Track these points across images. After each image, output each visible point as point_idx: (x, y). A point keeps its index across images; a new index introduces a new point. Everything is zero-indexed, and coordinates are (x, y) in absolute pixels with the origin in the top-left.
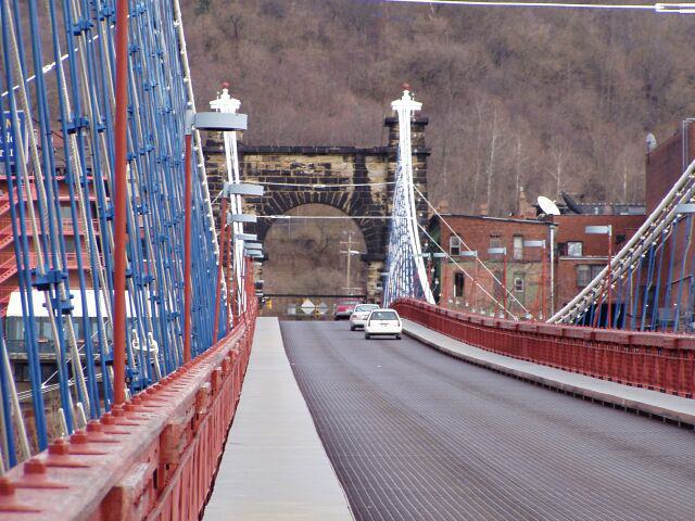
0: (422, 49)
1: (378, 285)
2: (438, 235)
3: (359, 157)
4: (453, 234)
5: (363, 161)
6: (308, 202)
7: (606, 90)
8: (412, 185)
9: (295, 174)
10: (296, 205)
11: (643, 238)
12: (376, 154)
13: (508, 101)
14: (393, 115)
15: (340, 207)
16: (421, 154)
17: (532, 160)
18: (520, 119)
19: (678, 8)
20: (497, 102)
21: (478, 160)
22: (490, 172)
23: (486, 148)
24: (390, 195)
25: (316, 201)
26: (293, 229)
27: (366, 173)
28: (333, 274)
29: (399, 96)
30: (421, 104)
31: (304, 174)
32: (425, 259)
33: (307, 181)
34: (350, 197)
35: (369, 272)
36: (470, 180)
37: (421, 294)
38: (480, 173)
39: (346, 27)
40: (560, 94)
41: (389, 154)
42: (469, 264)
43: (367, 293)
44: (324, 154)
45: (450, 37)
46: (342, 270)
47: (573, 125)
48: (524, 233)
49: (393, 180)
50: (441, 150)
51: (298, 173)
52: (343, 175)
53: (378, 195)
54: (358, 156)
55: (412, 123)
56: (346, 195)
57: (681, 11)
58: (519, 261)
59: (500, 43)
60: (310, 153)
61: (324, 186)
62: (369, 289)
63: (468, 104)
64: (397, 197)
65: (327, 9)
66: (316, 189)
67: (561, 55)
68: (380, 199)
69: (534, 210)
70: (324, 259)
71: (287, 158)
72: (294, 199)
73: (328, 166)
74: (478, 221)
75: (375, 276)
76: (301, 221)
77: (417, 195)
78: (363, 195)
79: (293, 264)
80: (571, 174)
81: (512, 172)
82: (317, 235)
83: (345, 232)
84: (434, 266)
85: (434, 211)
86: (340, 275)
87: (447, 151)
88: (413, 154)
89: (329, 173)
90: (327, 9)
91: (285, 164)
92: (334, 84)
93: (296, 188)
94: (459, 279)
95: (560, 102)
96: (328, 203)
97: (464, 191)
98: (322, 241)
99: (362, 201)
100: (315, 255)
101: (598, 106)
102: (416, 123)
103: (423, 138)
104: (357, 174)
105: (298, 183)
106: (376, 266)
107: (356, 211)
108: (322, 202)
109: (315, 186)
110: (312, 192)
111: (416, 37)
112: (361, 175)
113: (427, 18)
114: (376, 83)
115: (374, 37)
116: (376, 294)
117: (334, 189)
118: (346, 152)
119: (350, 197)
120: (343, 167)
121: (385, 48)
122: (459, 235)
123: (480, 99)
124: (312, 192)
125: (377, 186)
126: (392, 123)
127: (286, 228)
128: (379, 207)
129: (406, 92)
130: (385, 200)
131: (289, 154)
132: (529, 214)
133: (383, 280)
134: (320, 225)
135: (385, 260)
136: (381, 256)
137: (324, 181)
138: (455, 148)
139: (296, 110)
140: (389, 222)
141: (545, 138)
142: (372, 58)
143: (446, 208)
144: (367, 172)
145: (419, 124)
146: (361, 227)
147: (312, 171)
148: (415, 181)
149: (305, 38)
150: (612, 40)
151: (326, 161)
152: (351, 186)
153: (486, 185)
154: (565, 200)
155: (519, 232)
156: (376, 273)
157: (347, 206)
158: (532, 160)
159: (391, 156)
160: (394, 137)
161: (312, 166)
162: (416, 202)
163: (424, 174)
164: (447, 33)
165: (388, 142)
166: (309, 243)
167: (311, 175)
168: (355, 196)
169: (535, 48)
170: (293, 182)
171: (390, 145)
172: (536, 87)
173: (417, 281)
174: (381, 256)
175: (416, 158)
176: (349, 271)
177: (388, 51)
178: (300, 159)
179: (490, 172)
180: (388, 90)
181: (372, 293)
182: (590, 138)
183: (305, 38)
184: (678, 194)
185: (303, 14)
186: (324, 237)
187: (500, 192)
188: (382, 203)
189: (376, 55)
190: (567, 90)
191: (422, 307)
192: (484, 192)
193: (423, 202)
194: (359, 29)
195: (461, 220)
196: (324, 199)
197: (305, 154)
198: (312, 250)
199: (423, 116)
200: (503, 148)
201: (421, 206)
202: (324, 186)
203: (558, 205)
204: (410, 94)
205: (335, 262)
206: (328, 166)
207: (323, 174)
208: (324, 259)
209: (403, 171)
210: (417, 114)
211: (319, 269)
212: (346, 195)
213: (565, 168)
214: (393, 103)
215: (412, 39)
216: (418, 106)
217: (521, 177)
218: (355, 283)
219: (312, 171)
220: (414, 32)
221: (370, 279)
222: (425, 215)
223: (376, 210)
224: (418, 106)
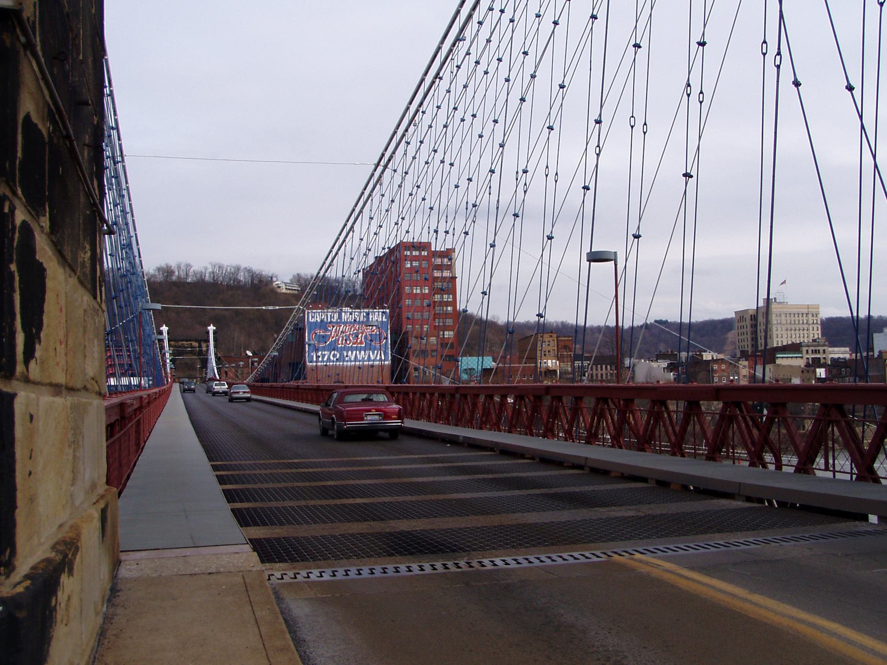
23: (234, 338)
29: (210, 326)
41: (208, 341)
54: (199, 342)
85: (219, 355)
94: (226, 373)
99: (200, 353)
106: (204, 370)
112: (200, 346)
118: (196, 341)
120: (195, 344)
125: (204, 349)
126: (208, 333)
133: (206, 373)
135: (207, 368)
140: (207, 358)
145: (215, 332)
178: (184, 342)
196: (191, 353)
216: (215, 328)
224: (215, 328)
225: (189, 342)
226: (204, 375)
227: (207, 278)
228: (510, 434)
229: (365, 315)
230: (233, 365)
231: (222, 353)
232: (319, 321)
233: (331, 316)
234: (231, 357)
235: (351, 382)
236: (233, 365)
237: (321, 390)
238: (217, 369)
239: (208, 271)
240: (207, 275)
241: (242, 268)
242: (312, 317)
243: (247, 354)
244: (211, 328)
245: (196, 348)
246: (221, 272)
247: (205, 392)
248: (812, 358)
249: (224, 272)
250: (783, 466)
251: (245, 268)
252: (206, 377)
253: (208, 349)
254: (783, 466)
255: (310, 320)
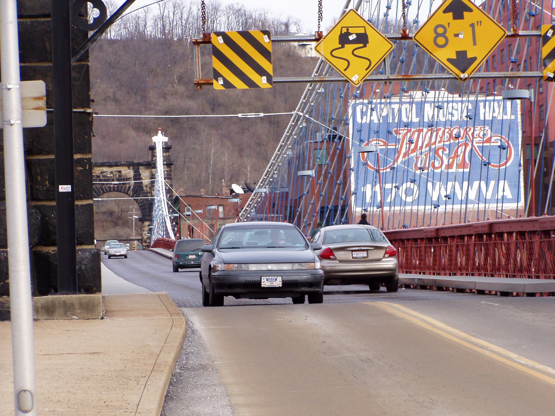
0: (171, 103)
1: (148, 233)
2: (179, 206)
3: (136, 167)
4: (186, 206)
5: (138, 169)
6: (110, 191)
7: (274, 123)
8: (163, 181)
9: (103, 177)
10: (104, 193)
11: (251, 203)
12: (145, 165)
13: (220, 131)
14: (153, 144)
15: (127, 193)
16: (168, 164)
17: (233, 164)
18: (228, 143)
19: (247, 115)
20: (214, 132)
21: (203, 165)
22: (210, 171)
23: (208, 158)
24: (153, 186)
25: (114, 191)
26: (102, 206)
27: (140, 175)
28: (125, 230)
29: (156, 134)
30: (167, 138)
31: (107, 177)
32: (170, 217)
33: (109, 180)
34: (132, 188)
35: (143, 227)
36: (200, 175)
37: (167, 234)
38: (205, 172)
39: (128, 92)
40: (249, 126)
41: (151, 165)
42: (196, 221)
43: (143, 238)
44: (117, 166)
45: (187, 97)
46: (130, 227)
47: (256, 143)
48: (224, 204)
49: (155, 178)
50: (182, 159)
51: (104, 176)
52: (128, 177)
53: (146, 186)
54: (136, 166)
55: (163, 148)
56: (130, 187)
57: (248, 116)
58: (221, 219)
59: (214, 99)
60: (110, 166)
61: (118, 183)
62: (143, 235)
63: (197, 134)
64: (156, 187)
65: (118, 83)
66: (114, 184)
67: (248, 105)
68: (148, 188)
69: (229, 191)
70: (120, 222)
71: (98, 169)
72: (103, 190)
73: (120, 172)
74: (200, 199)
75: (146, 229)
76: (107, 201)
77: (166, 185)
78: (138, 187)
79: (103, 226)
80: (256, 170)
81: (223, 170)
82: (116, 209)
83: (131, 207)
84: (176, 222)
85: (176, 194)
86: (129, 230)
87: (186, 160)
88: (164, 164)
89: (120, 176)
90: (118, 83)
91: (97, 172)
92: (123, 125)
93: (103, 184)
94: (191, 230)
95: (248, 130)
96: (121, 192)
97: (197, 182)
98: (118, 212)
99: (138, 190)
100: (115, 220)
101: (270, 132)
102: (165, 148)
103: (169, 156)
104: (135, 176)
105: (104, 181)
106: (147, 223)
107: (135, 195)
108: (117, 191)
109: (113, 183)
110: (112, 186)
111: (168, 97)
112: (137, 176)
113: (173, 87)
114: (146, 124)
115: (144, 98)
116: (147, 238)
117: (123, 184)
118: (129, 165)
119: (132, 188)
120: (128, 172)
121: (150, 104)
122: (189, 205)
123: (204, 131)
124: (112, 186)
125: (146, 181)
126: (153, 149)
127: (99, 205)
128: (147, 193)
129: (160, 132)
130: (150, 189)
131: (99, 166)
132: (226, 194)
133: (150, 230)
134: (117, 203)
135: (151, 221)
136: (149, 218)
137: (118, 180)
138: (191, 159)
139: (102, 140)
140: (153, 200)
141: (241, 151)
142: (143, 109)
143: (183, 192)
144: (141, 174)
145: (167, 148)
146: (138, 204)
147: (112, 175)
148: (165, 179)
149: (105, 100)
150: (277, 95)
151: (119, 170)
152: (132, 182)
153: (209, 178)
154: (246, 185)
155: (221, 203)
156: (147, 227)
157: (131, 192)
158: (233, 164)
159: (152, 166)
160: (154, 156)
161: (112, 173)
162: (166, 189)
163: (170, 175)
164: (184, 94)
165: (151, 158)
166: (111, 213)
167: (111, 177)
168: (134, 187)
169: (234, 101)
170: (102, 181)
171: (152, 160)
172: (235, 122)
173: (166, 230)
174: (149, 218)
175: (166, 166)
176: (134, 228)
177: (152, 106)
178: (105, 169)
179: (210, 171)
180: (153, 127)
181: (145, 237)
182: (265, 150)
183: (105, 100)
184: (261, 185)
185: (103, 86)
186: (120, 210)
187: (216, 182)
188: (149, 190)
189: (146, 108)
190: (252, 124)
191: (168, 241)
192: (208, 182)
193: (169, 189)
194: (135, 94)
195: (191, 198)
196: (119, 189)
197: (108, 166)
198: (113, 217)
199: (169, 144)
200: (217, 157)
201: (169, 191)
202: (118, 183)
203: (243, 189)
204: (162, 133)
205: (126, 223)
206: (120, 172)
207: (117, 176)
208: (120, 222)
209: (159, 174)
210: (166, 143)
211: (117, 228)
212: (130, 187)
213: (252, 168)
214: (153, 138)
215: (165, 98)
216: (166, 139)
217: (227, 173)
218: (137, 234)
219: (112, 175)
220: (167, 94)
221: (144, 230)
222: (171, 196)
223: (146, 194)
224: (166, 139)
225: (115, 169)
226: (146, 235)
227: (150, 30)
228: (493, 278)
229: (470, 107)
230: (200, 211)
231: (182, 190)
232: (376, 121)
233: (362, 110)
234: (201, 197)
235: (463, 220)
236: (200, 211)
237: (445, 239)
238: (172, 222)
239: (150, 16)
240: (149, 24)
241: (222, 7)
242: (363, 114)
243: (232, 191)
244: (159, 140)
245: (128, 179)
246: (178, 16)
247: (172, 269)
248: (333, 135)
249: (185, 16)
250: (324, 296)
251: (230, 8)
252: (150, 238)
253: (153, 183)
254: (324, 296)
255: (359, 120)
